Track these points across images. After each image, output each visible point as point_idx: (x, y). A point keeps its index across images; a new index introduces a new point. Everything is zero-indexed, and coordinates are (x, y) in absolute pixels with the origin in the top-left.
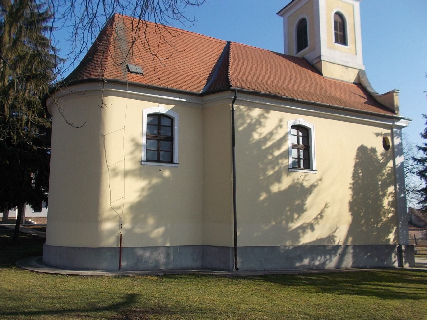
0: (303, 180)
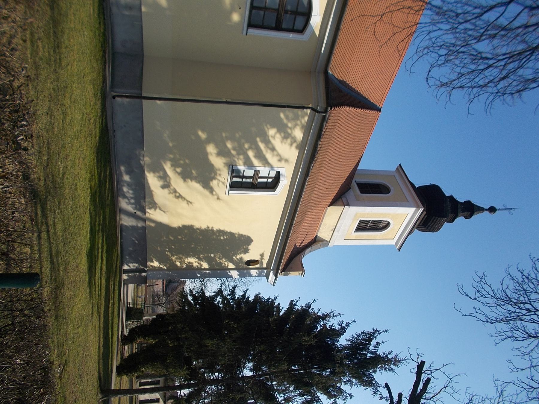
0: (219, 180)
